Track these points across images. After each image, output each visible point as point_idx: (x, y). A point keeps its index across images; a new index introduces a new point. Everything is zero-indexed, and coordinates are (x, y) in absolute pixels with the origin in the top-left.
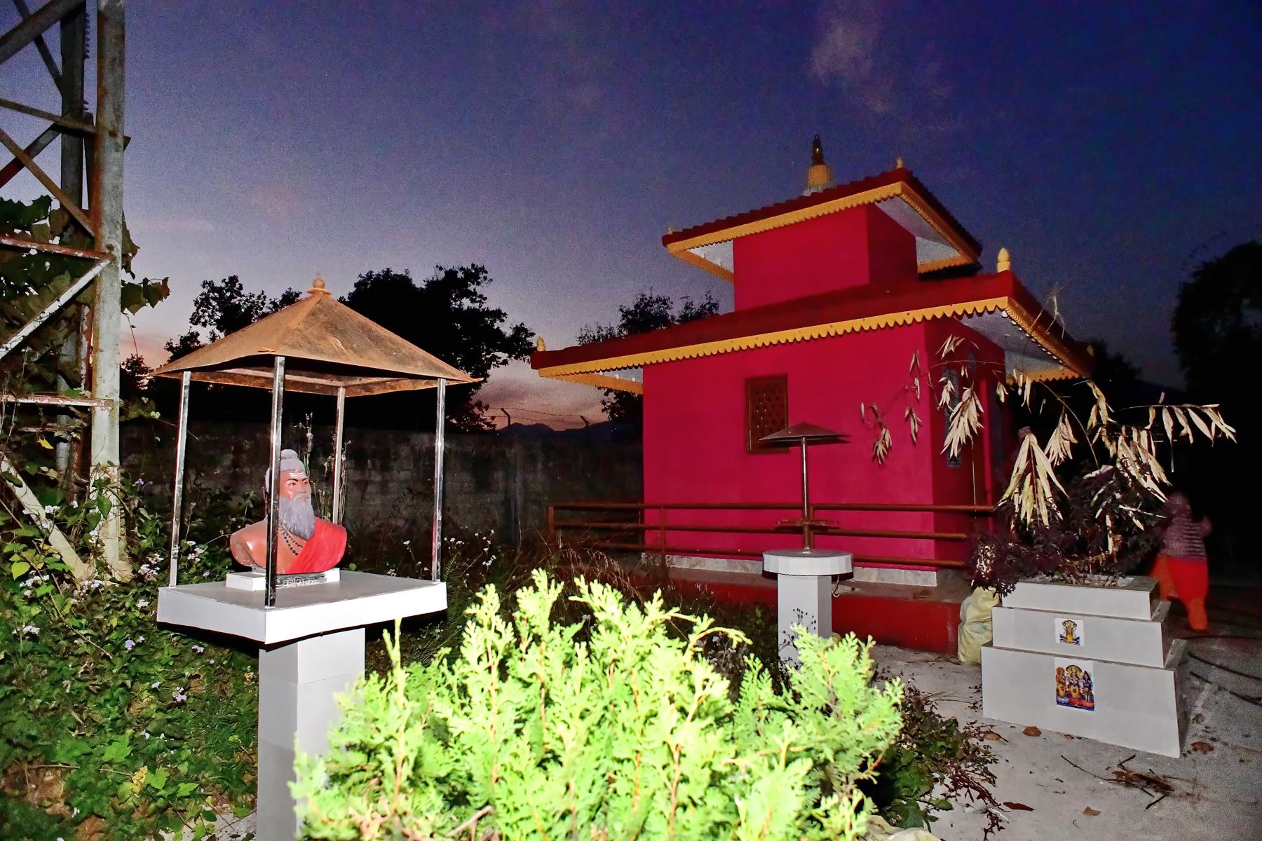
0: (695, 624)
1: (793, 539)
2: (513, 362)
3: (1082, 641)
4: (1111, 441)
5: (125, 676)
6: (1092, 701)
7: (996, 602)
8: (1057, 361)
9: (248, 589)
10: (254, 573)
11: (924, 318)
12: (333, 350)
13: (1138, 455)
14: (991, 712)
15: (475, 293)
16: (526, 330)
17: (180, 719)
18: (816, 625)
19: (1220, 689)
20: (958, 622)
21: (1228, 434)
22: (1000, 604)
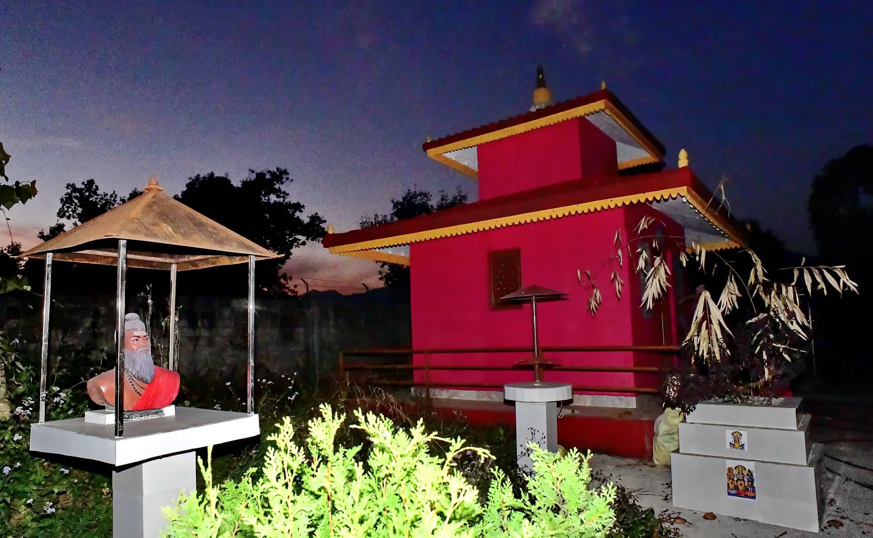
0: (450, 444)
1: (527, 374)
2: (309, 242)
3: (746, 447)
4: (766, 295)
5: (6, 494)
6: (754, 491)
7: (681, 418)
8: (723, 235)
9: (103, 423)
10: (107, 410)
11: (624, 203)
12: (166, 235)
13: (786, 306)
14: (678, 502)
15: (279, 190)
16: (319, 218)
17: (51, 526)
18: (545, 440)
19: (847, 479)
20: (652, 435)
21: (853, 288)
22: (684, 420)
